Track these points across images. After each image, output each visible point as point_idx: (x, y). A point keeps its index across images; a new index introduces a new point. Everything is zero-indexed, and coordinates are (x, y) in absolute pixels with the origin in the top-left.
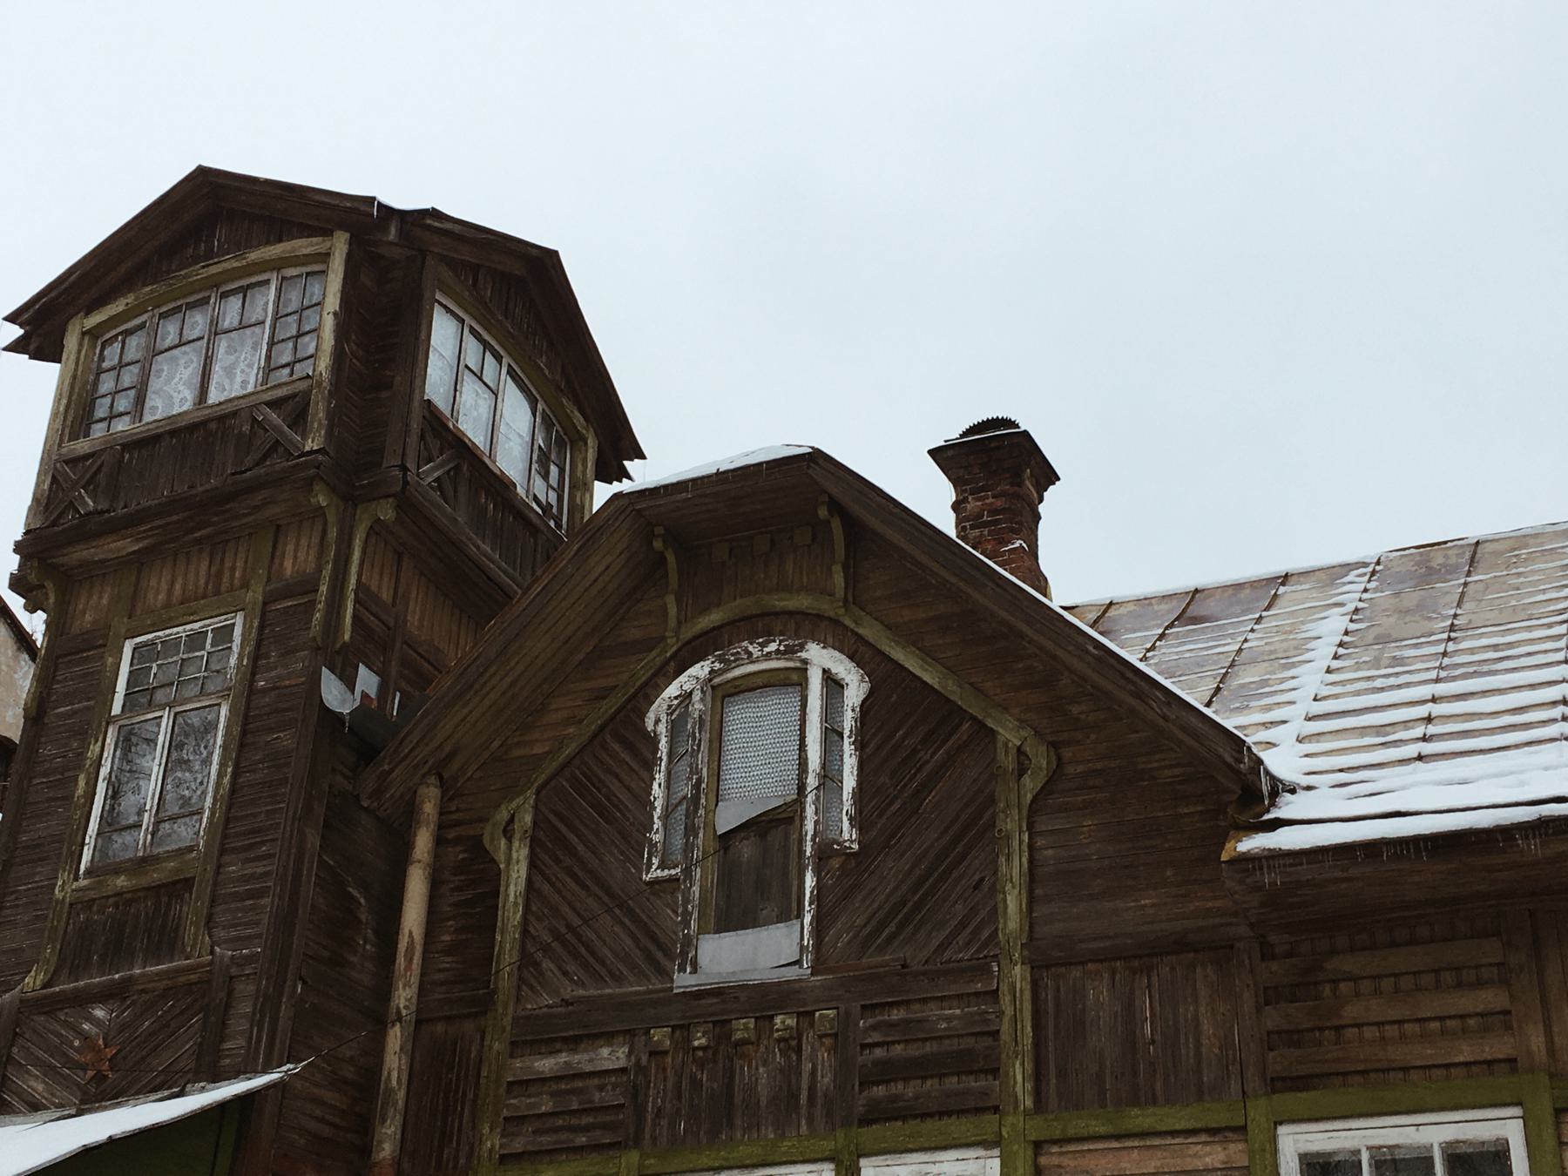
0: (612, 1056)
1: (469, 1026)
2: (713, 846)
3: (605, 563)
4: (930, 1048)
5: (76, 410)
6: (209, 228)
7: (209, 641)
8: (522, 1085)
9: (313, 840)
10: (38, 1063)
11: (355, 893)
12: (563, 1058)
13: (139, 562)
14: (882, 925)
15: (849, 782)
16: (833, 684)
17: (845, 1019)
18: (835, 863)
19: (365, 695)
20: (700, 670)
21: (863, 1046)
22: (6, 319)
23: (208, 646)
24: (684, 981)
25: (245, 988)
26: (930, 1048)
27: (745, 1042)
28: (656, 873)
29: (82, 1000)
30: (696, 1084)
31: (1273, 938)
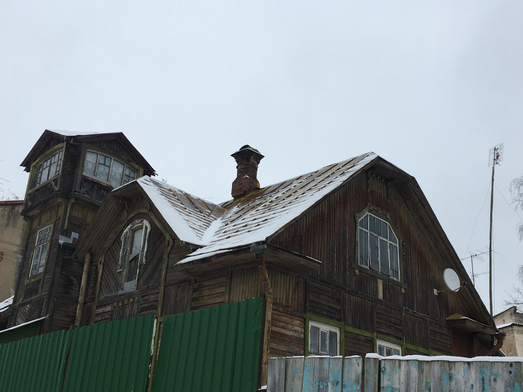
0: (109, 308)
1: (92, 303)
2: (128, 263)
3: (111, 206)
4: (150, 304)
5: (32, 183)
6: (49, 141)
7: (384, 239)
8: (97, 315)
9: (58, 269)
10: (20, 316)
11: (73, 278)
12: (103, 309)
13: (41, 215)
14: (147, 279)
15: (146, 250)
16: (146, 228)
17: (139, 299)
18: (142, 267)
19: (74, 238)
20: (129, 227)
21: (141, 304)
22: (21, 165)
23: (386, 240)
24: (120, 292)
25: (45, 300)
26: (150, 304)
27: (126, 305)
28: (119, 270)
29: (26, 304)
30: (120, 313)
31: (197, 279)
